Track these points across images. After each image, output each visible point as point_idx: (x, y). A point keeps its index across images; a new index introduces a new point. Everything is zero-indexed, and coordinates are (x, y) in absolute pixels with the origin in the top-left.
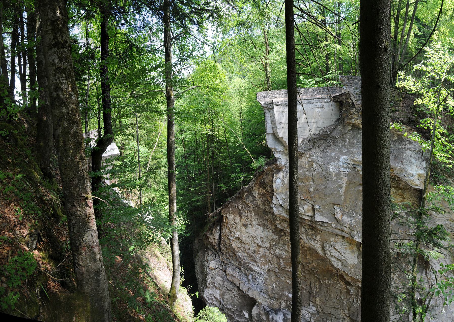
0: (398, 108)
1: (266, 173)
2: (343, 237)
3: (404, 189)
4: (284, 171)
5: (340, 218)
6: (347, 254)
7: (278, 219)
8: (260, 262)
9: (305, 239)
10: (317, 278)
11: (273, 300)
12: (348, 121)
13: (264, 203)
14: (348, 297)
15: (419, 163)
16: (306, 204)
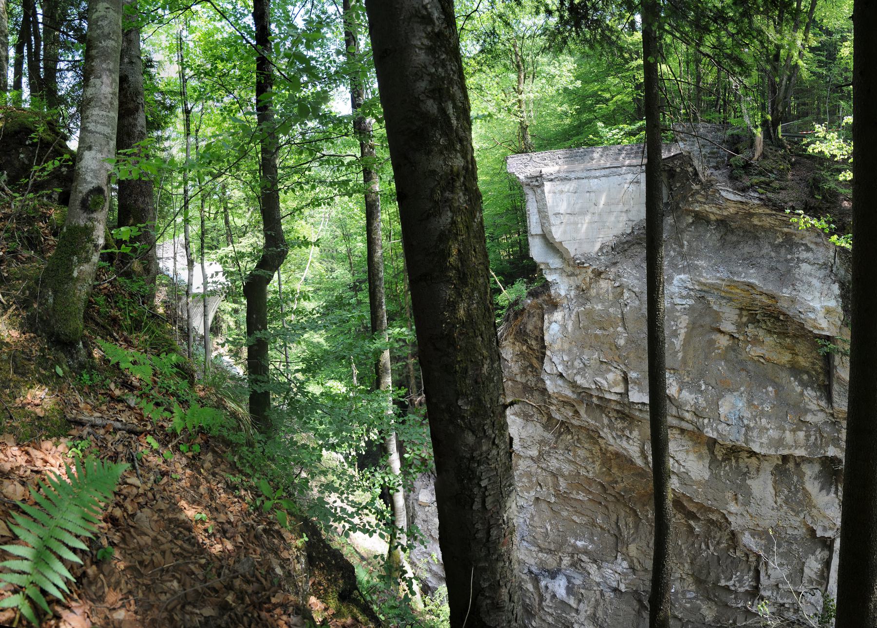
0: (783, 184)
1: (529, 312)
2: (682, 431)
4: (564, 308)
5: (676, 395)
7: (555, 402)
9: (610, 437)
10: (631, 509)
11: (547, 553)
12: (687, 207)
13: (524, 372)
14: (691, 540)
15: (826, 287)
16: (611, 371)
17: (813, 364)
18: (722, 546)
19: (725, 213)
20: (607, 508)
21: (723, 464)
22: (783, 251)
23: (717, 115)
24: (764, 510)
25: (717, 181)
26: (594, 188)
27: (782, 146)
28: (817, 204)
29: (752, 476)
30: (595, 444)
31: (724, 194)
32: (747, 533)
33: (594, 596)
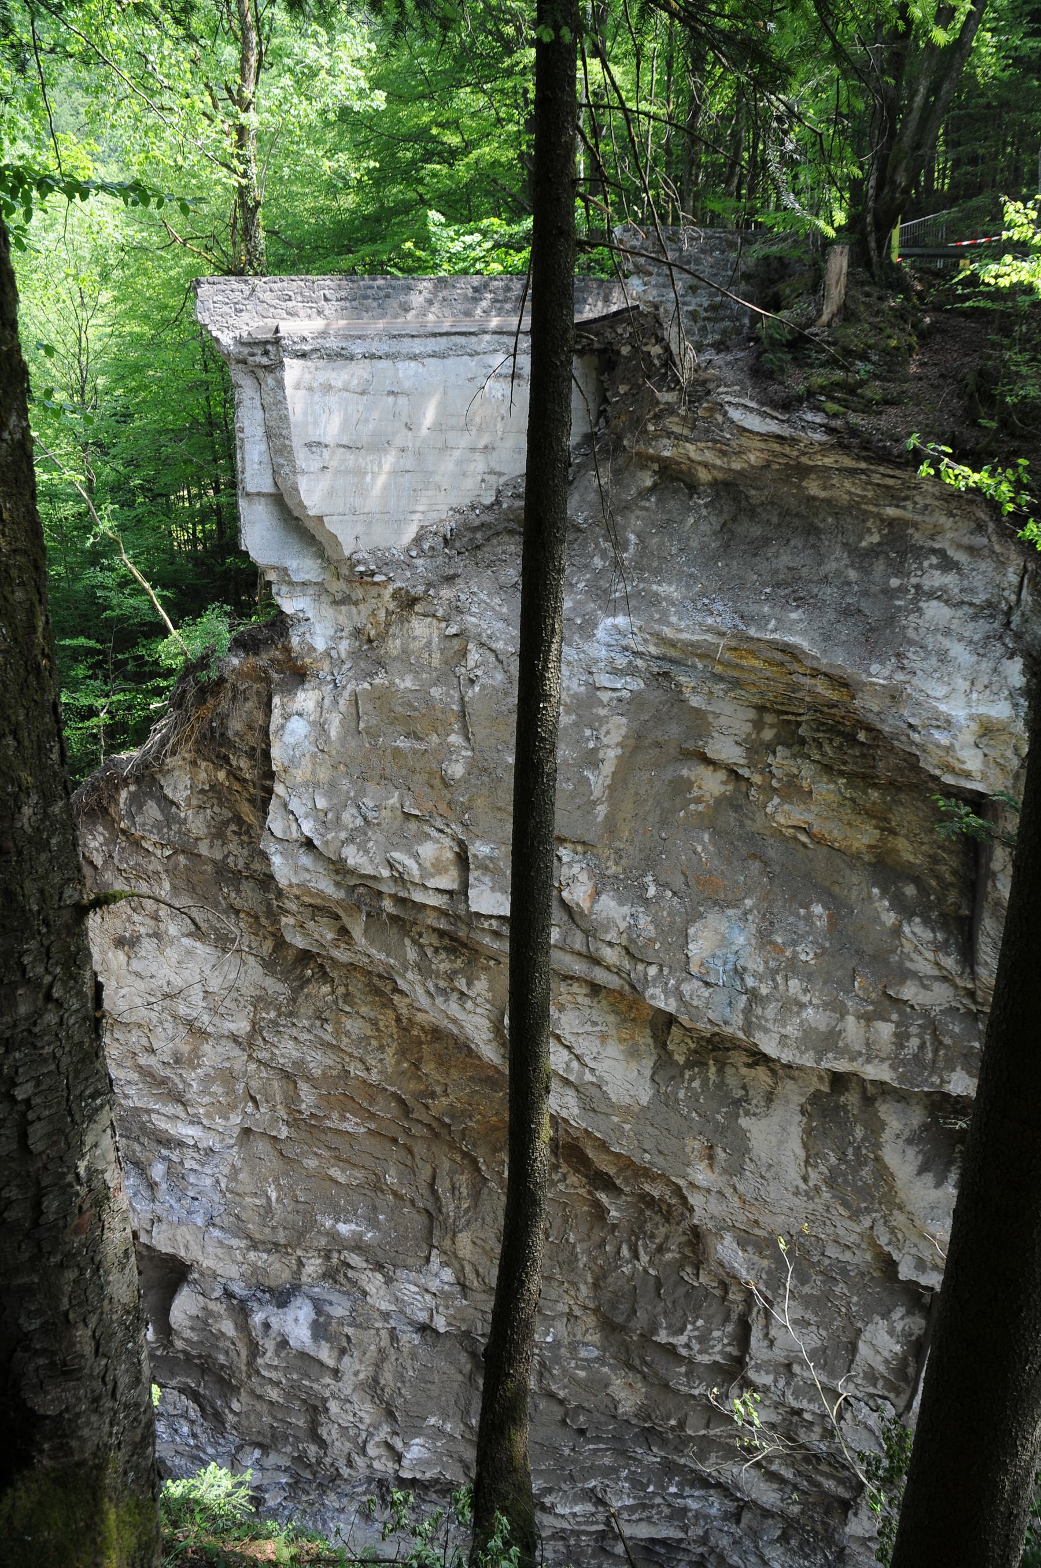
0: (894, 389)
1: (234, 687)
2: (595, 989)
3: (893, 786)
4: (322, 682)
5: (585, 905)
6: (608, 1062)
7: (292, 906)
8: (206, 1100)
9: (420, 991)
10: (466, 1155)
11: (269, 1252)
12: (641, 447)
13: (218, 834)
14: (598, 1234)
15: (986, 665)
16: (428, 836)
17: (935, 860)
18: (669, 1256)
19: (737, 466)
20: (410, 1151)
21: (687, 1074)
22: (879, 567)
23: (732, 203)
24: (773, 1192)
25: (720, 381)
26: (407, 384)
27: (899, 285)
28: (984, 442)
29: (753, 1109)
30: (384, 1006)
31: (735, 414)
32: (728, 1238)
33: (373, 1342)
